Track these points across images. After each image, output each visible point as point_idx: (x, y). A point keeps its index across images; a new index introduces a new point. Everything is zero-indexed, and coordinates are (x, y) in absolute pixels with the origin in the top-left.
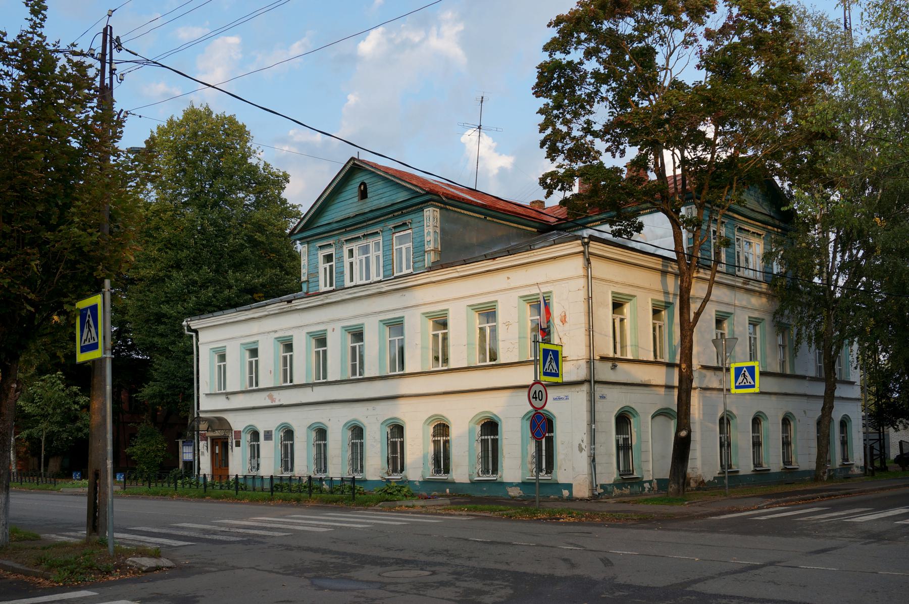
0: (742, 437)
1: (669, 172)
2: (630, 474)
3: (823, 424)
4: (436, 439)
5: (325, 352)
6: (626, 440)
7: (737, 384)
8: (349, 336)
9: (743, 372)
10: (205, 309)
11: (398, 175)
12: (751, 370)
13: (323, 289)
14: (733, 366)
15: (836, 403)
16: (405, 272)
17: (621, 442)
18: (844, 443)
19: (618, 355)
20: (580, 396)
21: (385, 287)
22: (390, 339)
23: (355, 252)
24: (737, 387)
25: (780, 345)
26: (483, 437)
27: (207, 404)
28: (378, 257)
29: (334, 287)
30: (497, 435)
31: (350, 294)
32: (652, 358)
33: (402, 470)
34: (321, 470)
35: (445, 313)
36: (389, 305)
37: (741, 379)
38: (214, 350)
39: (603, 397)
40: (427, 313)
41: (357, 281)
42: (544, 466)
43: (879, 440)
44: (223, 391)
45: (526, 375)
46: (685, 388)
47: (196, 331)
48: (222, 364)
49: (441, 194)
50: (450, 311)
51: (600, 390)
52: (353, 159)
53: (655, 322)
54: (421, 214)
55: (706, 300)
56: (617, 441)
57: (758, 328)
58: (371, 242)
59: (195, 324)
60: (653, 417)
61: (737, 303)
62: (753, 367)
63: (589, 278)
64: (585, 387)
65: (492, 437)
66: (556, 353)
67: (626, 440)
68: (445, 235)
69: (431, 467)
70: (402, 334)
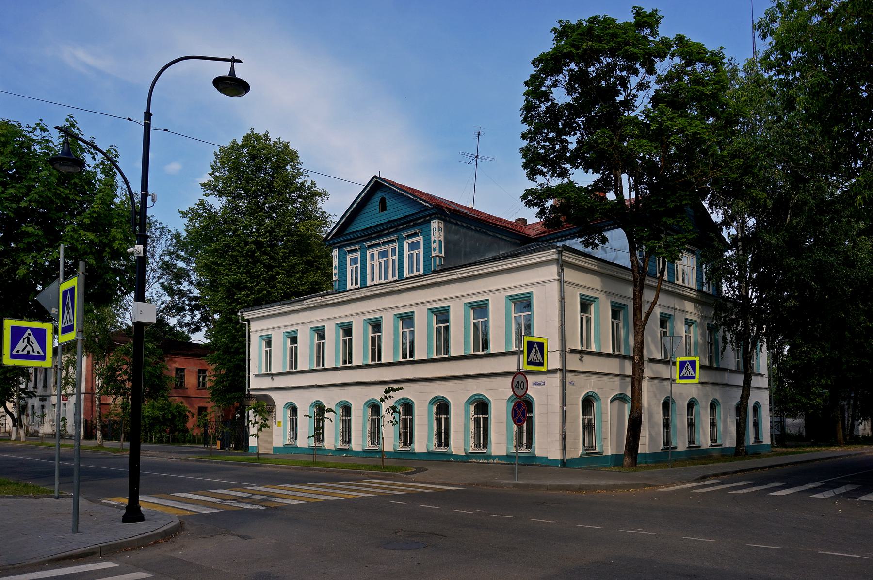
0: (680, 421)
1: (626, 196)
2: (593, 450)
3: (741, 409)
4: (439, 416)
5: (350, 340)
6: (590, 420)
7: (529, 360)
8: (342, 331)
9: (686, 365)
10: (258, 303)
11: (410, 192)
12: (40, 335)
13: (349, 287)
14: (678, 360)
15: (752, 392)
16: (415, 273)
17: (586, 422)
18: (756, 424)
19: (584, 348)
20: (555, 380)
21: (399, 286)
22: (403, 330)
23: (376, 256)
24: (681, 378)
25: (708, 343)
26: (476, 416)
27: (255, 384)
28: (394, 261)
29: (359, 285)
30: (488, 414)
31: (371, 291)
32: (611, 352)
33: (411, 442)
34: (345, 442)
35: (529, 296)
36: (436, 296)
37: (684, 371)
38: (263, 337)
39: (572, 383)
40: (315, 327)
41: (377, 281)
42: (525, 442)
43: (780, 422)
44: (269, 372)
45: (511, 365)
46: (636, 380)
47: (248, 321)
48: (269, 349)
49: (444, 209)
50: (451, 307)
51: (570, 377)
52: (375, 177)
53: (613, 320)
54: (428, 224)
55: (654, 304)
56: (583, 421)
57: (692, 328)
58: (389, 248)
59: (247, 315)
60: (612, 401)
61: (677, 307)
62: (695, 362)
63: (561, 282)
64: (558, 376)
65: (483, 416)
66: (541, 346)
67: (590, 420)
68: (449, 244)
69: (435, 441)
70: (413, 326)
